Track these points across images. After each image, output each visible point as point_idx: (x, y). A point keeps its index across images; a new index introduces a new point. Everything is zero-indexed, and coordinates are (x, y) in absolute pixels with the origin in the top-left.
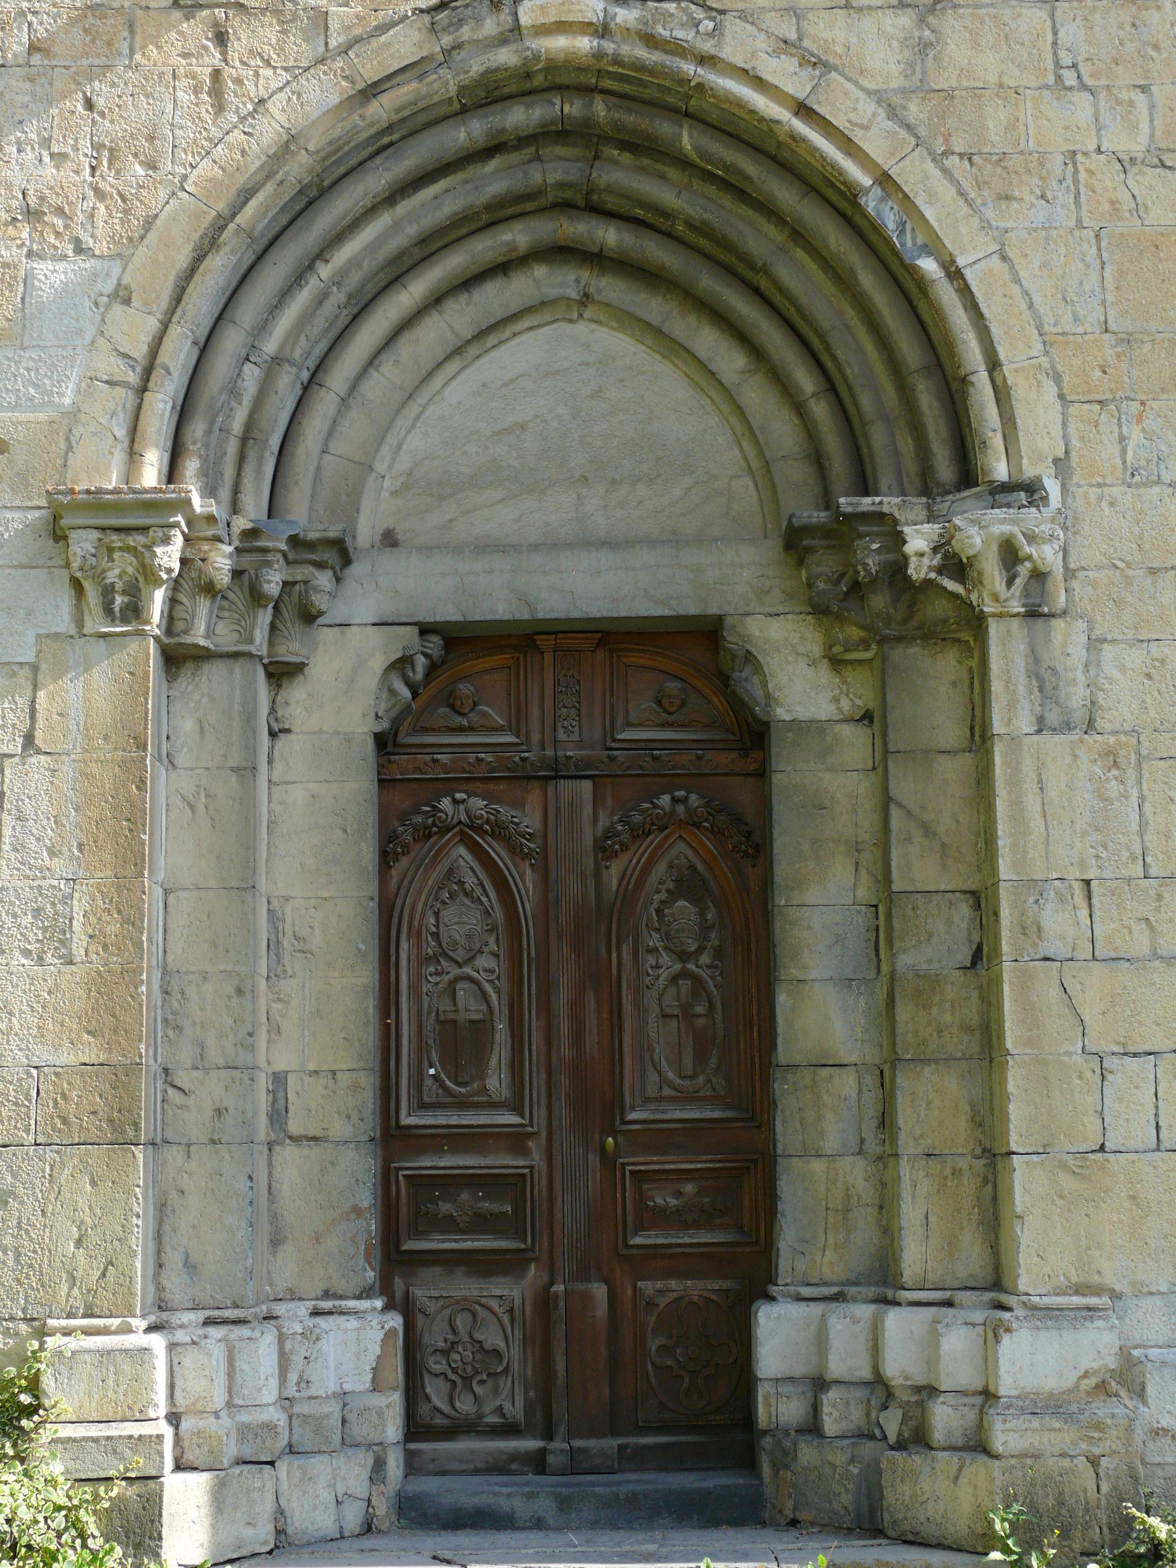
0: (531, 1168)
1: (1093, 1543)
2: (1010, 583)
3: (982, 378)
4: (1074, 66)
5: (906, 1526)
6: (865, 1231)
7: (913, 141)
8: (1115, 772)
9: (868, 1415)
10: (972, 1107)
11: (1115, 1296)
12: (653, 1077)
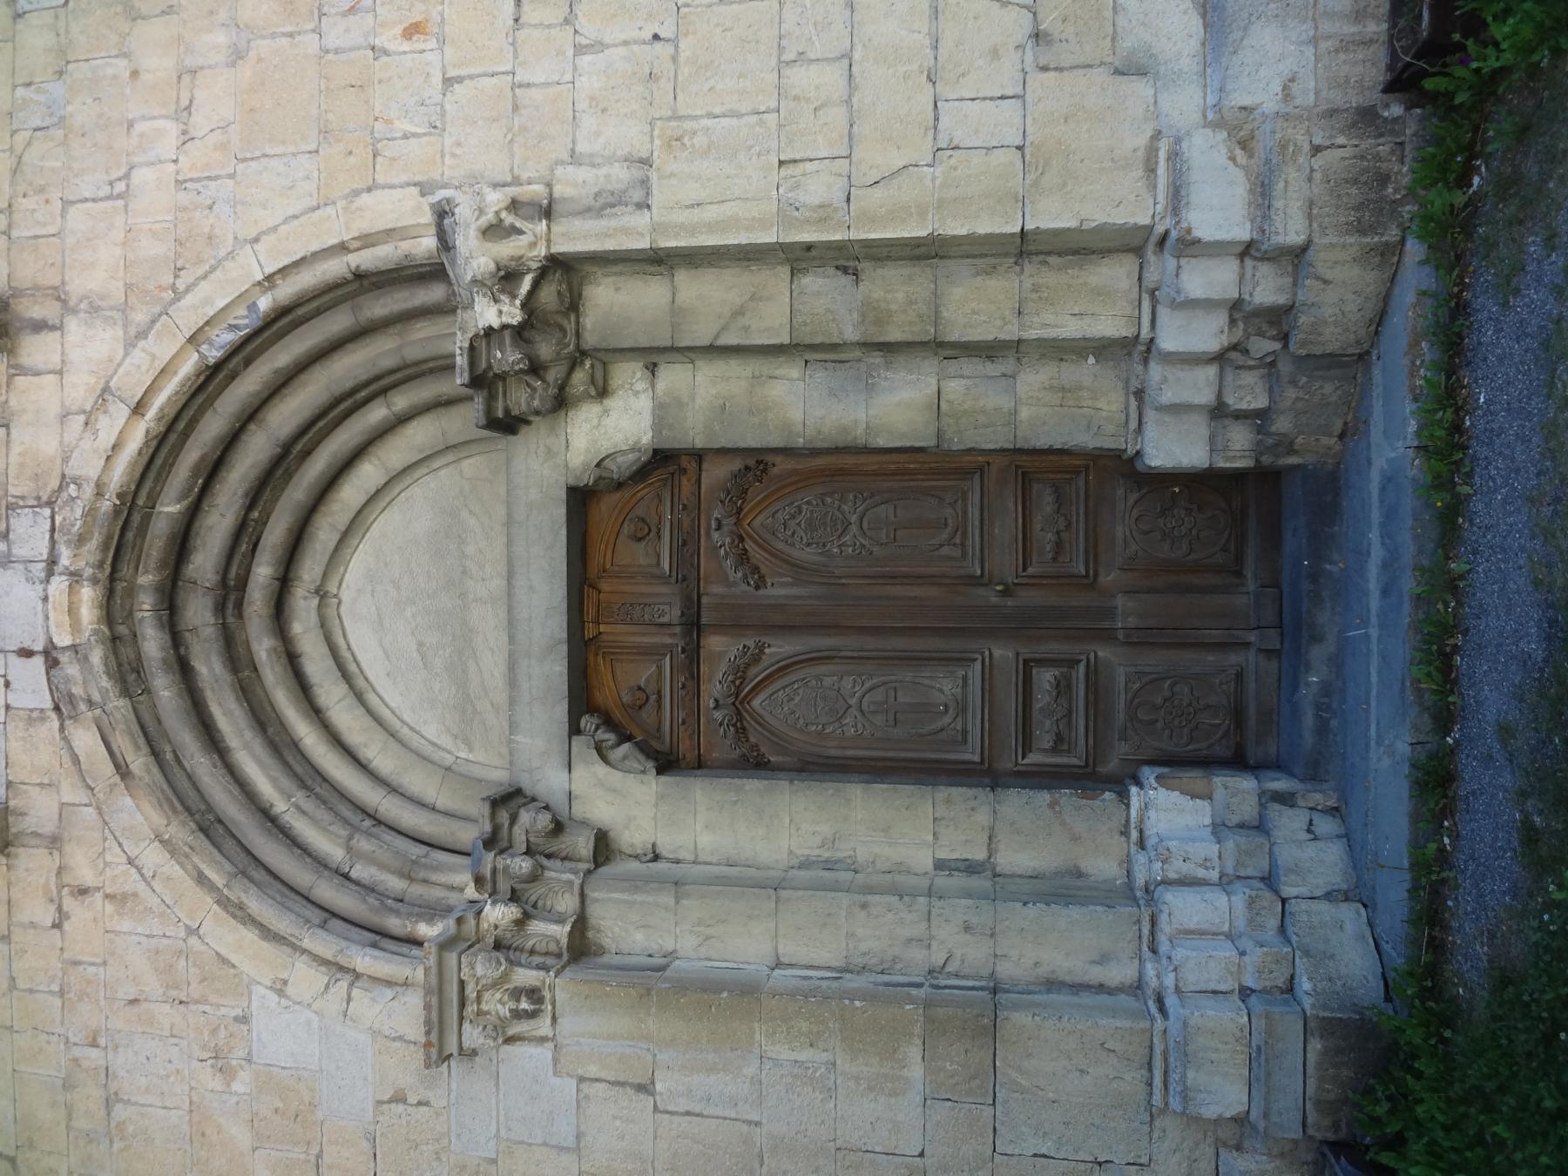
1: (1393, 152)
2: (520, 232)
4: (111, 184)
5: (1362, 332)
6: (1087, 371)
7: (165, 317)
8: (686, 140)
9: (1250, 368)
10: (978, 274)
11: (1157, 135)
12: (945, 550)
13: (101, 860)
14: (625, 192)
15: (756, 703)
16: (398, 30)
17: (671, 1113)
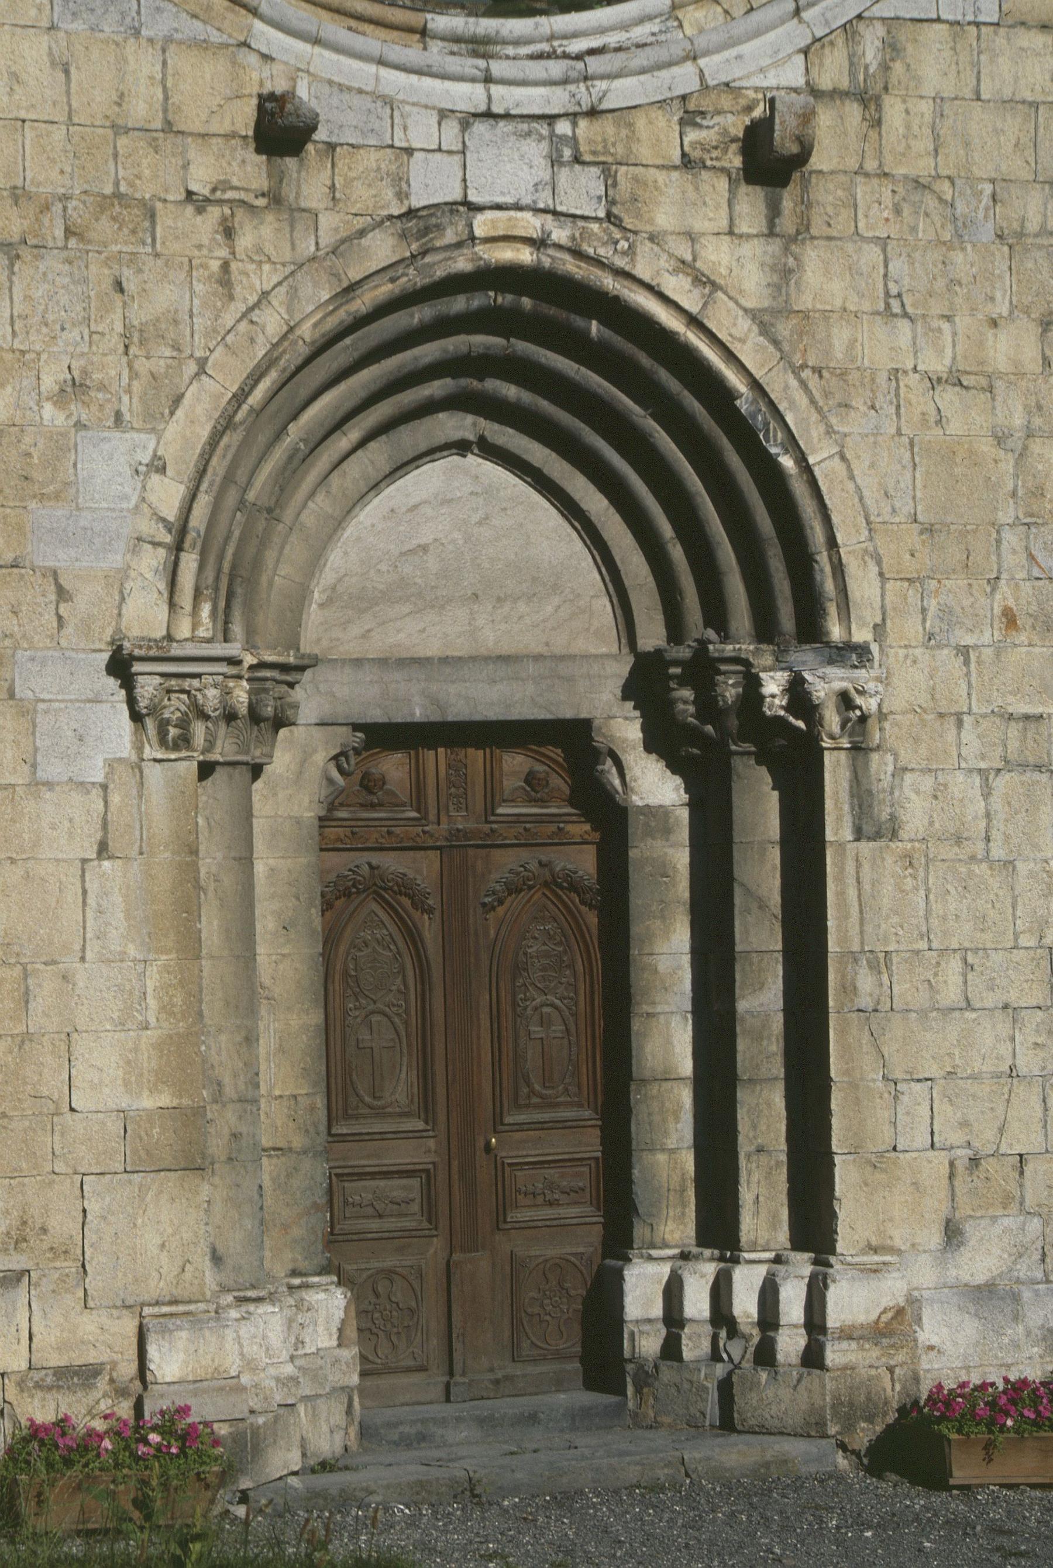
0: (434, 1163)
3: (823, 559)
4: (899, 295)
5: (753, 1422)
8: (910, 871)
11: (899, 1252)
13: (264, 259)
14: (872, 818)
15: (374, 906)
16: (1011, 603)
17: (83, 876)
